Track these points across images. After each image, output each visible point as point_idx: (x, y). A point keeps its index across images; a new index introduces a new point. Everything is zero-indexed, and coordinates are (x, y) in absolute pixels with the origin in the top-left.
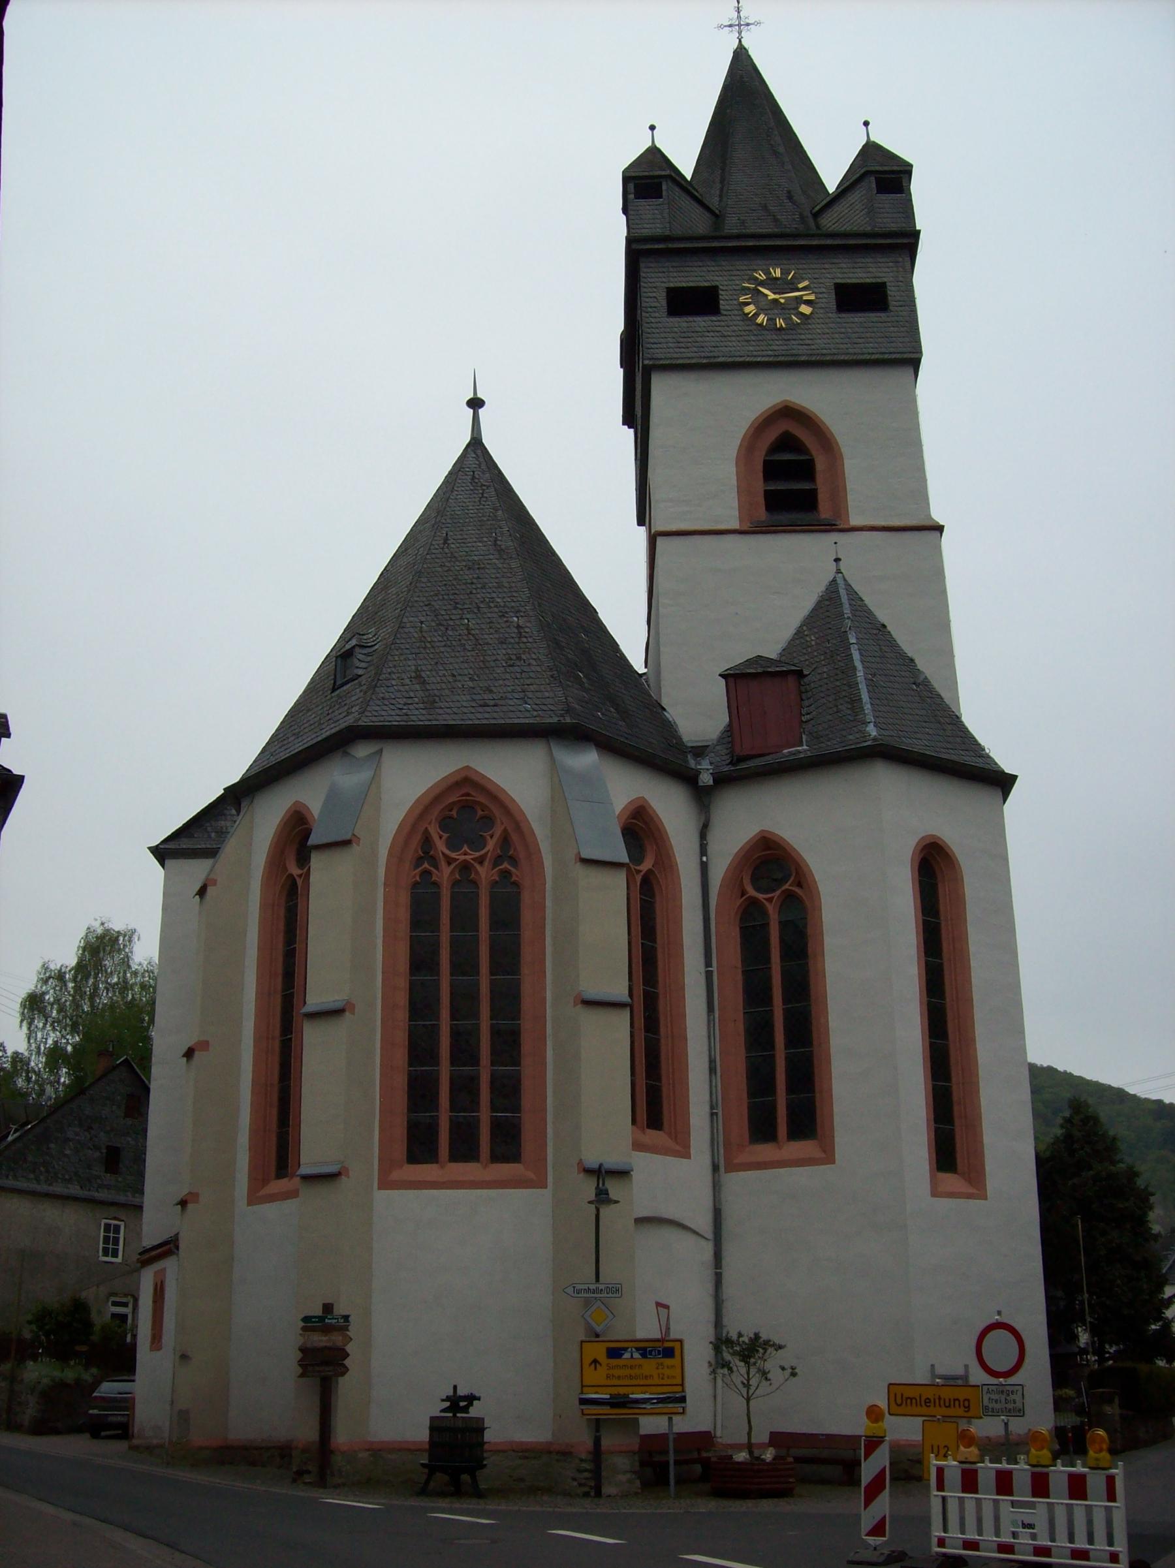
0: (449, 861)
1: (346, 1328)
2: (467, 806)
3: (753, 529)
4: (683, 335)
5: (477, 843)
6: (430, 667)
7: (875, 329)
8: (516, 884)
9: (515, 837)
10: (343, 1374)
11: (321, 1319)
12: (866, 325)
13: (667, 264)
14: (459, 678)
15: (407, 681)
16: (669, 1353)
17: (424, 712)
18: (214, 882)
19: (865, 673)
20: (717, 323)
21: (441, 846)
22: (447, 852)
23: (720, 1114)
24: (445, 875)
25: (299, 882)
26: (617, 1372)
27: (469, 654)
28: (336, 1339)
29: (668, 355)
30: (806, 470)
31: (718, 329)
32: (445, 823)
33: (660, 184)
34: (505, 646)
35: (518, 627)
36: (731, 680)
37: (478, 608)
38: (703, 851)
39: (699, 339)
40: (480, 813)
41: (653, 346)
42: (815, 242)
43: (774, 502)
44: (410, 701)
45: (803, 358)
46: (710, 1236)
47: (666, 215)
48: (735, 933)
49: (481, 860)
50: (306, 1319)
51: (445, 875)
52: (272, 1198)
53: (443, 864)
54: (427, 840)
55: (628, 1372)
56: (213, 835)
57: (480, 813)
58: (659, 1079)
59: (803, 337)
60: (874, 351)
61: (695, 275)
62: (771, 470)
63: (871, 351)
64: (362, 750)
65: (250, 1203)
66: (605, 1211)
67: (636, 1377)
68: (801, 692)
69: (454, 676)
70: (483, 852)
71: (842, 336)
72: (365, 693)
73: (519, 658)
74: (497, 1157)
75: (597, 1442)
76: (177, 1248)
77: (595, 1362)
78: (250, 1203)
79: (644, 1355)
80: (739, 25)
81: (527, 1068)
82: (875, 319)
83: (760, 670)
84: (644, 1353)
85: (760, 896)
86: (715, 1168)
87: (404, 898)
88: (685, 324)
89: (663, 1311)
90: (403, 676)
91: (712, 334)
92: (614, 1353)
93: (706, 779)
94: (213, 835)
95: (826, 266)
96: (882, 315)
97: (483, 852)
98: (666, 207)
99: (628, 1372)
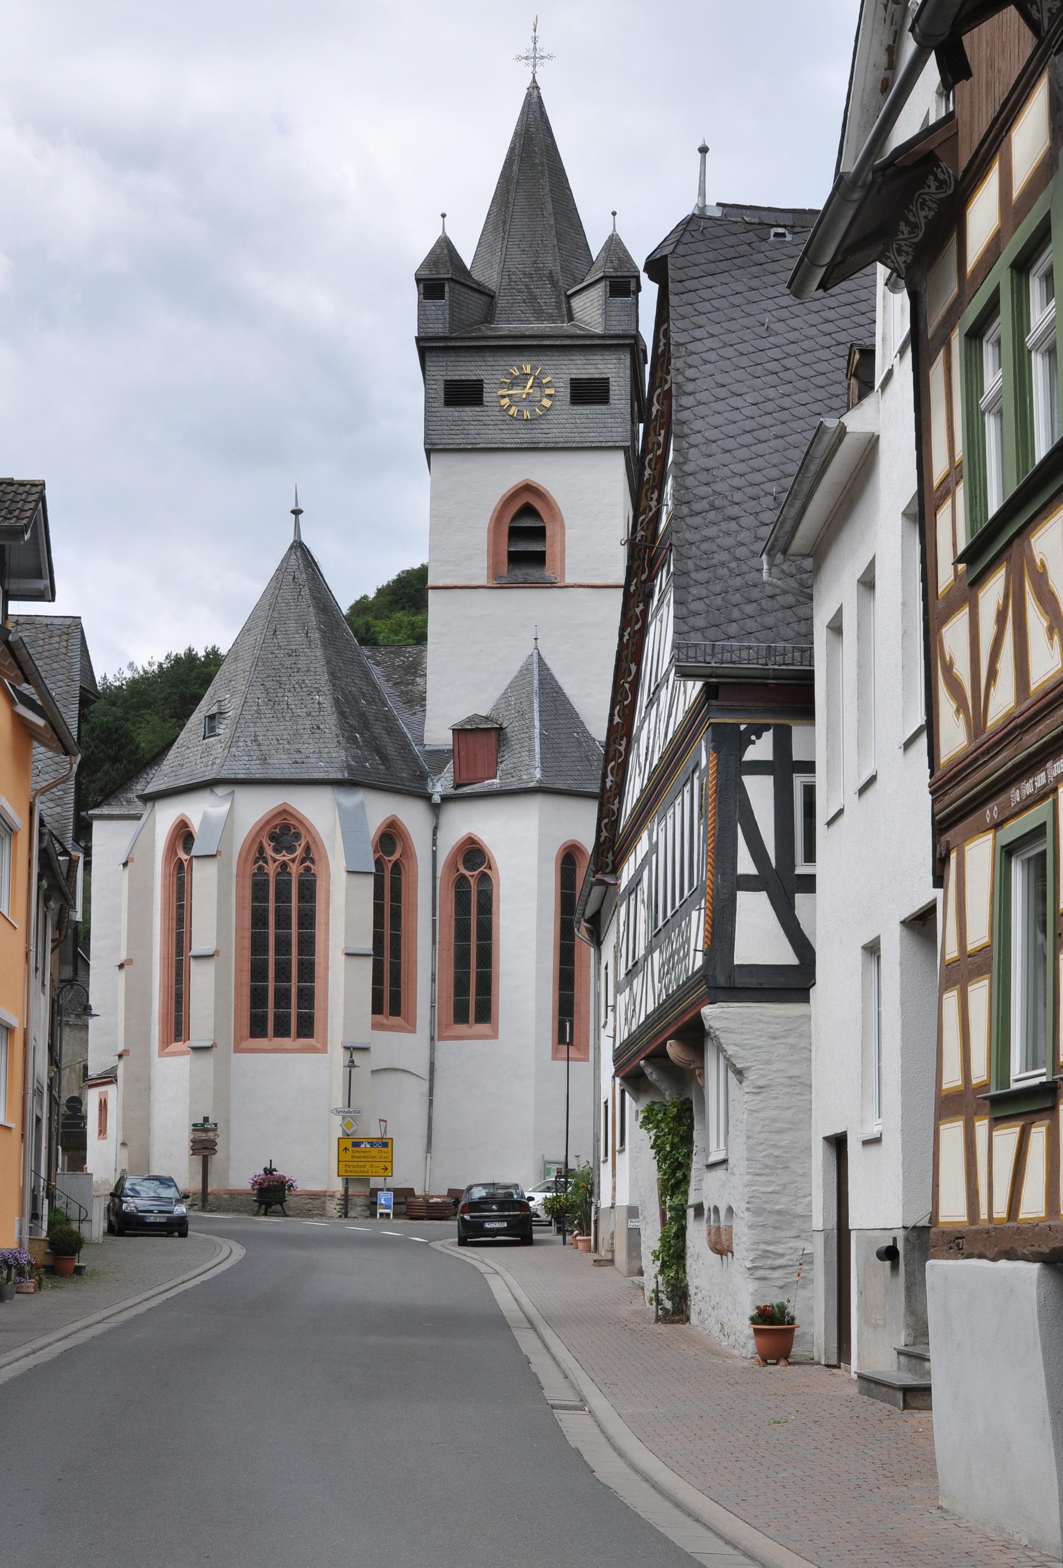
0: (275, 861)
1: (216, 1130)
2: (286, 828)
3: (500, 583)
4: (454, 423)
5: (291, 849)
6: (263, 733)
7: (597, 421)
8: (313, 875)
9: (312, 846)
10: (214, 1154)
11: (202, 1125)
12: (590, 416)
13: (445, 359)
14: (281, 741)
15: (249, 743)
16: (385, 1145)
17: (259, 767)
18: (132, 860)
19: (541, 730)
20: (480, 414)
21: (269, 852)
22: (274, 855)
23: (436, 1008)
24: (271, 869)
25: (186, 864)
26: (357, 1155)
27: (287, 723)
28: (211, 1134)
29: (443, 441)
30: (539, 533)
31: (480, 418)
32: (273, 837)
33: (443, 286)
34: (310, 718)
35: (319, 703)
36: (456, 732)
37: (294, 688)
38: (434, 844)
39: (466, 427)
40: (293, 831)
41: (433, 433)
42: (558, 343)
43: (516, 559)
44: (250, 758)
45: (541, 445)
46: (427, 1077)
47: (447, 316)
48: (452, 895)
49: (293, 860)
50: (194, 1125)
51: (271, 869)
52: (173, 1054)
53: (270, 862)
54: (261, 849)
55: (362, 1154)
56: (124, 803)
57: (293, 831)
58: (399, 986)
59: (543, 426)
60: (595, 439)
61: (466, 370)
62: (515, 533)
63: (591, 439)
64: (221, 791)
65: (160, 1056)
66: (353, 1070)
67: (368, 1157)
68: (499, 741)
69: (278, 740)
70: (295, 855)
71: (572, 426)
72: (224, 750)
73: (318, 728)
74: (300, 1035)
75: (346, 1190)
76: (116, 1081)
77: (346, 1149)
78: (160, 1056)
79: (372, 1146)
80: (535, 58)
81: (318, 985)
82: (599, 411)
83: (474, 727)
84: (372, 1145)
85: (467, 873)
86: (432, 1038)
87: (248, 884)
88: (456, 414)
89: (383, 1124)
90: (247, 739)
91: (476, 423)
92: (356, 1145)
93: (437, 799)
94: (124, 803)
95: (566, 362)
96: (603, 407)
97: (295, 855)
98: (447, 308)
99: (362, 1154)
